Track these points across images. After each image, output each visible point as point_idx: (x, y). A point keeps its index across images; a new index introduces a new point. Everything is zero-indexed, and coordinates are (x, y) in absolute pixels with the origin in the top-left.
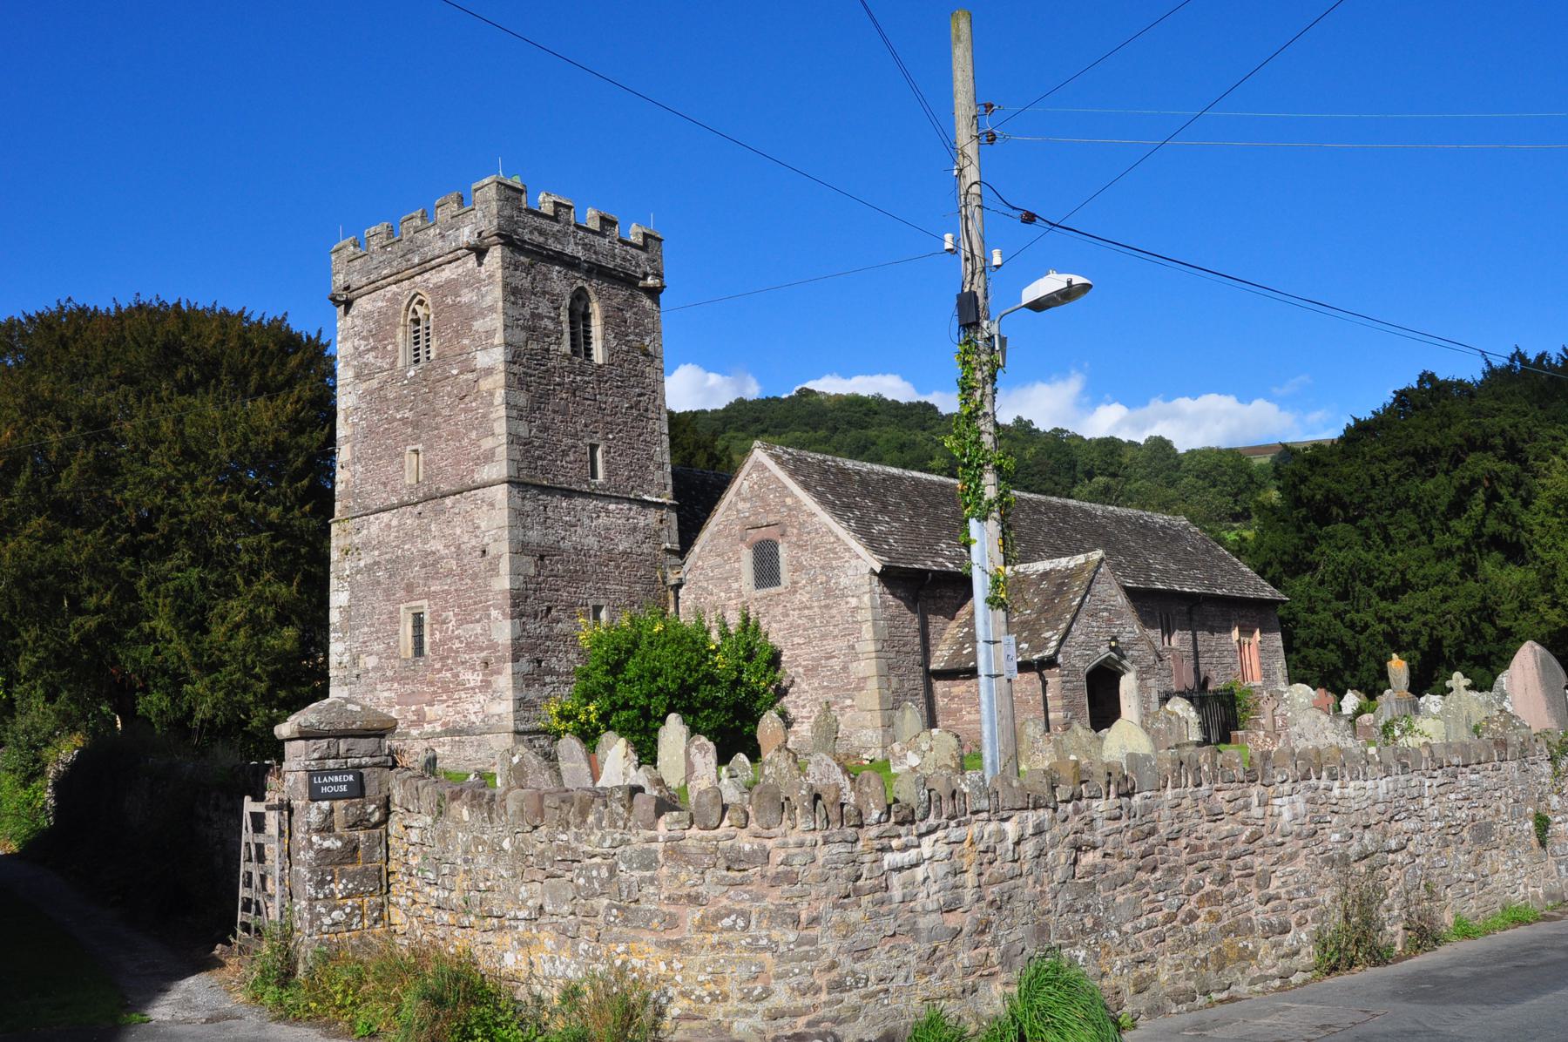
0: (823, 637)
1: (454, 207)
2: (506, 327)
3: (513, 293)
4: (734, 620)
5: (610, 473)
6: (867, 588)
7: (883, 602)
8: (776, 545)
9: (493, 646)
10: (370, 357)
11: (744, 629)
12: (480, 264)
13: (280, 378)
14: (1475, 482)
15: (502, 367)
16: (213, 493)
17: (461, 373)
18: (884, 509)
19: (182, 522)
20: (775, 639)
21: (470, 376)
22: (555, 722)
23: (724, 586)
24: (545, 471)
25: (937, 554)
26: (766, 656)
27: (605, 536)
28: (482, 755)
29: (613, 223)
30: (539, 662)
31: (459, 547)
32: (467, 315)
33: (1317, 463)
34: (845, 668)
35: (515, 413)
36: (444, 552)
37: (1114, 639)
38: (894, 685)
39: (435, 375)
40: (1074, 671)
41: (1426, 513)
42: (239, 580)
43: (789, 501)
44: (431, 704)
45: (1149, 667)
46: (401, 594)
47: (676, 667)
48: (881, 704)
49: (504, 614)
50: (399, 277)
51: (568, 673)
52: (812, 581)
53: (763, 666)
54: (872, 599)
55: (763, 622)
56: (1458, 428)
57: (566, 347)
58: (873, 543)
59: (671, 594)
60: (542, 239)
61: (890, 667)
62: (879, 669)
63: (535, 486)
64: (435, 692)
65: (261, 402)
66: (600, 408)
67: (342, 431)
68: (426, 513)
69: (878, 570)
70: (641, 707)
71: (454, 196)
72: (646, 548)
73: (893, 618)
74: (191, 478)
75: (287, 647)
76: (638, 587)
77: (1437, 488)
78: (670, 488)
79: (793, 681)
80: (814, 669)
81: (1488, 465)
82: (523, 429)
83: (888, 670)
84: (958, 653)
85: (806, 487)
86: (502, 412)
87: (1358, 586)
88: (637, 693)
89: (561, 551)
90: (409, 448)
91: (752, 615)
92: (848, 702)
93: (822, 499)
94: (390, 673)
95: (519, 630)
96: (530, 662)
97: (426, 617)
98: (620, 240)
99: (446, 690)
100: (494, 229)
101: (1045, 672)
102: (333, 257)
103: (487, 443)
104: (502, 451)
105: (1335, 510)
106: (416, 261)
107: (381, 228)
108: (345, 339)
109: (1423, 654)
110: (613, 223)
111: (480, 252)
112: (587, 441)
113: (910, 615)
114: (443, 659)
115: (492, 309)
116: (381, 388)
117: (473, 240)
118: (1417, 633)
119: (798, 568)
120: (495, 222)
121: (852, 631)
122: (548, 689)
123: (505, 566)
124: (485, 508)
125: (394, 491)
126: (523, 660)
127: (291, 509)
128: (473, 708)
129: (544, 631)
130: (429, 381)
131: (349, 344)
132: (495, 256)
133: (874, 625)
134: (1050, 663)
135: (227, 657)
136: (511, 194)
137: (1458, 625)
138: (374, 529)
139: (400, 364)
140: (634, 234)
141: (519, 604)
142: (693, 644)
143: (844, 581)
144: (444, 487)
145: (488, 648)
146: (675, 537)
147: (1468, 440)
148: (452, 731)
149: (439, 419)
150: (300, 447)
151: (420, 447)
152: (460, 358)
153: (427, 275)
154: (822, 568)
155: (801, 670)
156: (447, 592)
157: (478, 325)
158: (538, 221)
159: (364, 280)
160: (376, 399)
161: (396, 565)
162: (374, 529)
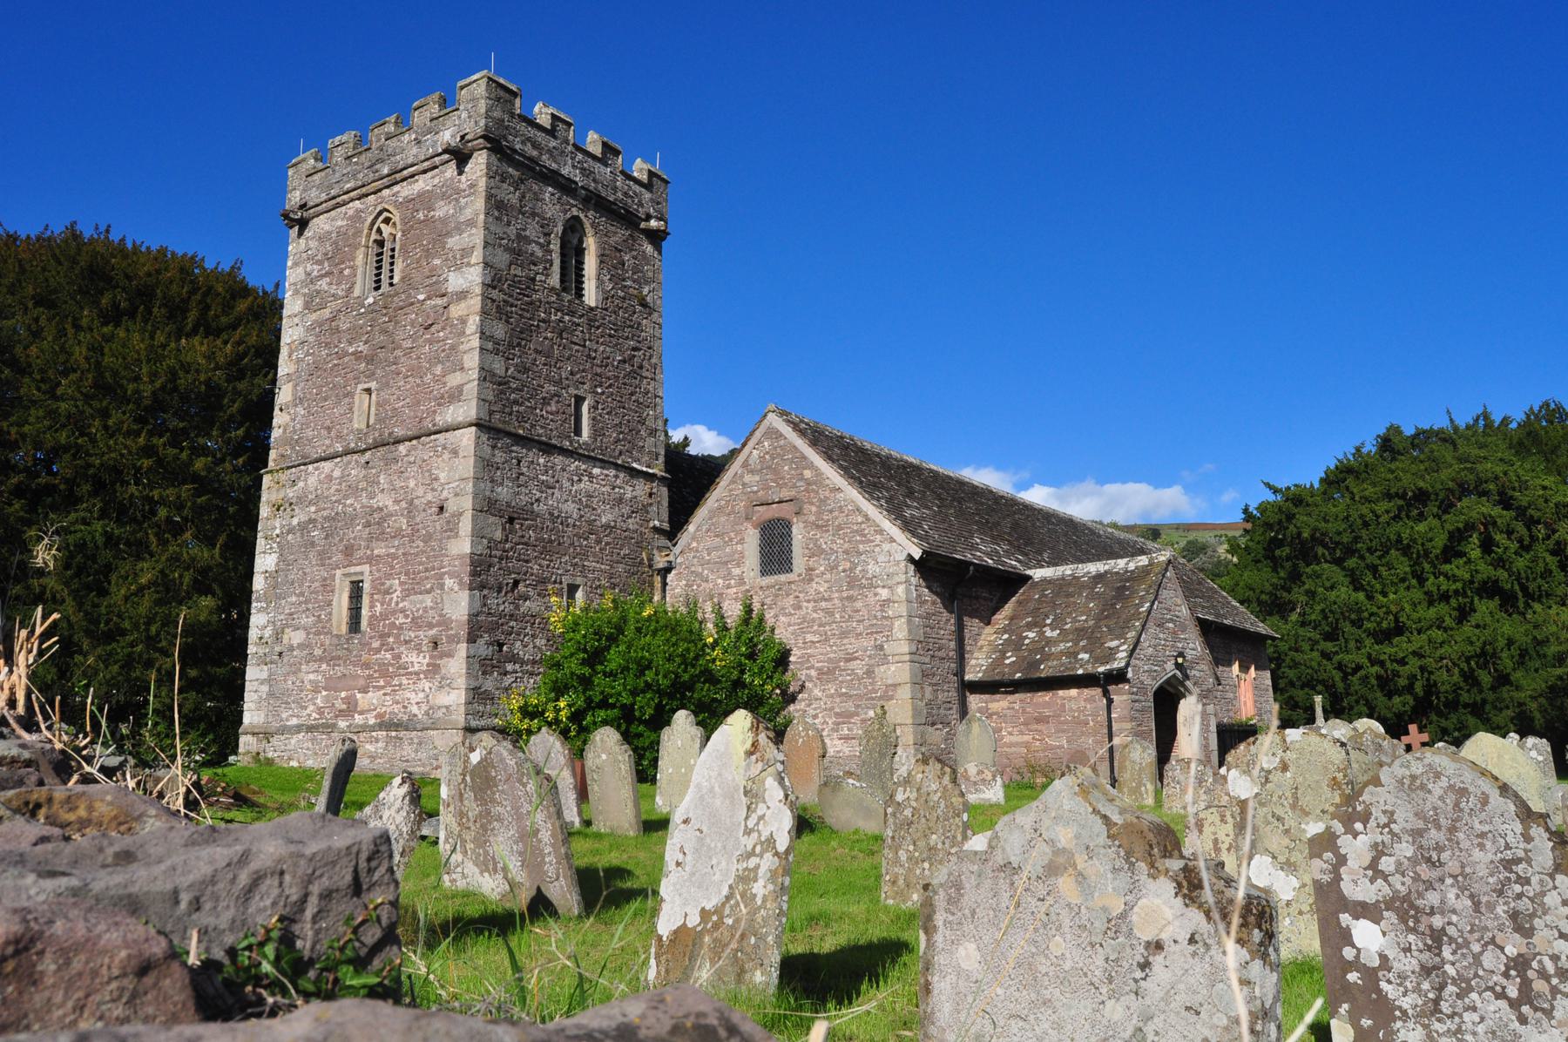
0: (844, 634)
1: (435, 109)
2: (486, 244)
3: (496, 206)
4: (733, 611)
5: (597, 432)
6: (902, 578)
7: (919, 596)
8: (788, 525)
9: (445, 622)
10: (323, 284)
11: (746, 620)
12: (460, 173)
13: (224, 320)
14: (1470, 527)
15: (478, 290)
16: (128, 433)
17: (429, 298)
18: (910, 493)
19: (89, 466)
20: (784, 634)
21: (439, 301)
22: (515, 720)
23: (723, 572)
24: (522, 419)
26: (772, 654)
27: (587, 503)
28: (422, 755)
29: (617, 153)
30: (501, 645)
31: (411, 503)
32: (441, 232)
33: (1301, 501)
34: (870, 673)
35: (490, 346)
36: (393, 508)
37: (1181, 654)
38: (928, 695)
39: (397, 301)
40: (1142, 689)
41: (1419, 556)
42: (152, 538)
43: (807, 474)
44: (364, 691)
45: (1209, 691)
46: (338, 557)
47: (670, 659)
48: (914, 717)
49: (461, 583)
50: (364, 190)
51: (534, 662)
53: (769, 666)
54: (908, 591)
55: (769, 616)
56: (1445, 474)
57: (555, 280)
58: (909, 526)
59: (658, 579)
60: (535, 153)
61: (925, 675)
62: (913, 675)
63: (509, 434)
64: (370, 677)
65: (196, 340)
66: (589, 356)
67: (284, 367)
68: (376, 462)
69: (917, 557)
70: (623, 706)
71: (436, 96)
72: (632, 523)
73: (928, 616)
74: (105, 414)
75: (202, 618)
76: (621, 568)
77: (1430, 530)
78: (661, 459)
79: (803, 686)
80: (830, 672)
81: (1484, 509)
82: (498, 366)
83: (923, 677)
84: (998, 662)
85: (829, 458)
86: (475, 342)
87: (1347, 627)
88: (619, 689)
89: (534, 515)
90: (360, 387)
91: (756, 606)
93: (846, 472)
94: (318, 652)
95: (478, 604)
96: (489, 644)
97: (366, 586)
98: (622, 172)
99: (384, 674)
100: (480, 131)
101: (1110, 688)
102: (290, 172)
103: (454, 380)
104: (472, 389)
105: (1320, 550)
106: (386, 171)
107: (348, 137)
108: (296, 264)
109: (1416, 698)
110: (617, 153)
111: (460, 156)
112: (572, 391)
113: (946, 614)
114: (383, 636)
115: (471, 223)
116: (333, 319)
117: (455, 142)
118: (1413, 678)
119: (815, 551)
120: (482, 123)
121: (880, 627)
122: (508, 680)
123: (466, 526)
124: (446, 456)
125: (339, 437)
126: (481, 642)
127: (222, 460)
128: (415, 698)
129: (508, 608)
130: (389, 312)
131: (300, 270)
132: (479, 163)
133: (909, 622)
134: (1119, 677)
135: (127, 625)
136: (502, 95)
137: (1456, 670)
138: (312, 481)
139: (357, 292)
140: (639, 169)
141: (481, 572)
142: (682, 630)
143: (872, 568)
144: (399, 432)
145: (439, 624)
146: (665, 515)
147: (1461, 485)
148: (388, 725)
149: (398, 353)
150: (237, 393)
151: (373, 385)
152: (429, 281)
153: (396, 188)
154: (846, 552)
155: (813, 673)
156: (394, 556)
157: (453, 242)
158: (532, 132)
159: (324, 196)
160: (327, 331)
161: (335, 523)
162: (312, 481)
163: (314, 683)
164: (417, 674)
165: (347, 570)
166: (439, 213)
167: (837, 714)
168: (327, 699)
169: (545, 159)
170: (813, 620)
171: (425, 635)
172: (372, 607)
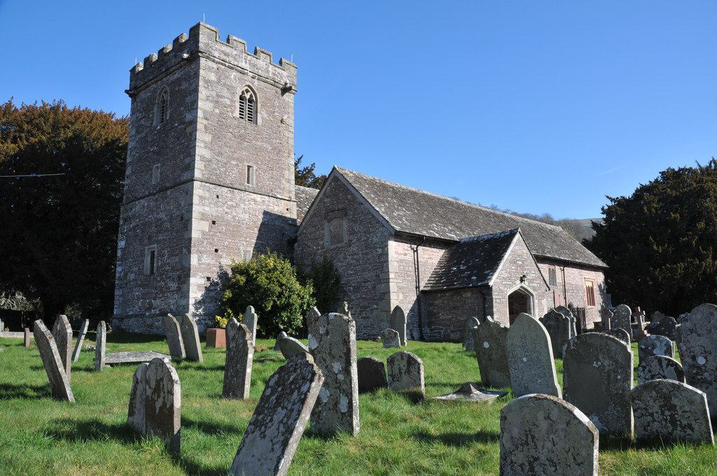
0: (364, 270)
17: (179, 125)
21: (182, 126)
25: (430, 229)
34: (374, 288)
43: (349, 197)
52: (359, 240)
57: (237, 114)
92: (375, 306)
116: (146, 136)
139: (154, 124)
144: (168, 185)
156: (165, 240)
163: (138, 296)
164: (173, 291)
165: (149, 247)
166: (183, 87)
167: (361, 307)
168: (142, 303)
169: (231, 59)
170: (351, 264)
171: (176, 274)
172: (158, 262)
